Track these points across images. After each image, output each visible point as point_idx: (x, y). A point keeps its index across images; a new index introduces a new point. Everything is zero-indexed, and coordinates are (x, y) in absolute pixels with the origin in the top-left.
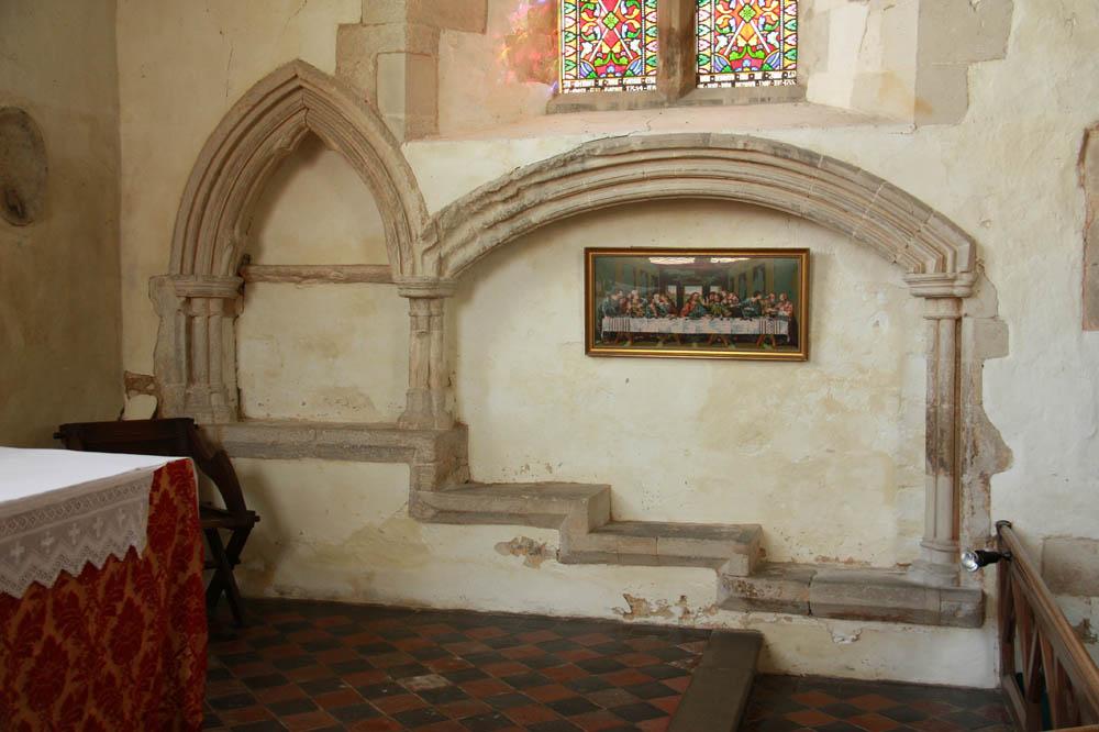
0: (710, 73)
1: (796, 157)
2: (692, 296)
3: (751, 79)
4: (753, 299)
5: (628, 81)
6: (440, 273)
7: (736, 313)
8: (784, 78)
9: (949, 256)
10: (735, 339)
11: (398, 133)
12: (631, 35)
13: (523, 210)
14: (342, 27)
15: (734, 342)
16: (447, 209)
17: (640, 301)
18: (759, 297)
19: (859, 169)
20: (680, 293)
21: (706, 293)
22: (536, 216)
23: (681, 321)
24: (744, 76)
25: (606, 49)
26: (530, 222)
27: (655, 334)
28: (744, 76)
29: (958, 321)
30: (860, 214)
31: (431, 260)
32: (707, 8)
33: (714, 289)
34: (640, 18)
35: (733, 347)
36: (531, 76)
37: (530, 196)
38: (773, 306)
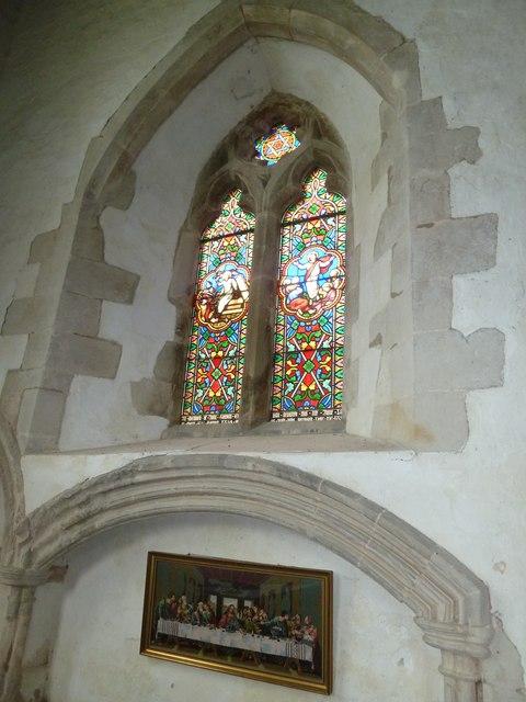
0: (279, 411)
1: (298, 479)
2: (229, 608)
3: (309, 415)
4: (281, 619)
5: (224, 417)
6: (28, 563)
7: (266, 631)
8: (334, 415)
9: (461, 603)
10: (264, 658)
11: (22, 447)
12: (229, 384)
13: (89, 516)
14: (10, 372)
15: (263, 661)
16: (38, 509)
17: (188, 607)
18: (286, 617)
19: (359, 495)
20: (220, 601)
21: (241, 606)
22: (99, 522)
23: (219, 631)
24: (304, 413)
25: (212, 394)
26: (93, 527)
27: (197, 641)
28: (304, 413)
29: (478, 683)
30: (362, 543)
31: (24, 550)
32: (280, 363)
33: (248, 604)
34: (234, 372)
35: (261, 667)
36: (151, 411)
37: (97, 504)
38: (298, 629)
